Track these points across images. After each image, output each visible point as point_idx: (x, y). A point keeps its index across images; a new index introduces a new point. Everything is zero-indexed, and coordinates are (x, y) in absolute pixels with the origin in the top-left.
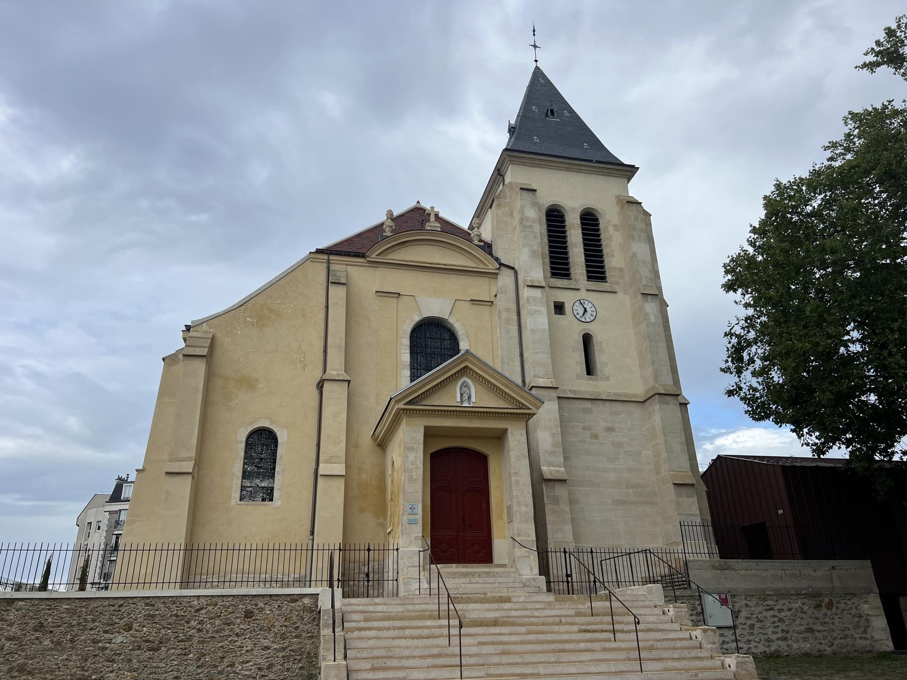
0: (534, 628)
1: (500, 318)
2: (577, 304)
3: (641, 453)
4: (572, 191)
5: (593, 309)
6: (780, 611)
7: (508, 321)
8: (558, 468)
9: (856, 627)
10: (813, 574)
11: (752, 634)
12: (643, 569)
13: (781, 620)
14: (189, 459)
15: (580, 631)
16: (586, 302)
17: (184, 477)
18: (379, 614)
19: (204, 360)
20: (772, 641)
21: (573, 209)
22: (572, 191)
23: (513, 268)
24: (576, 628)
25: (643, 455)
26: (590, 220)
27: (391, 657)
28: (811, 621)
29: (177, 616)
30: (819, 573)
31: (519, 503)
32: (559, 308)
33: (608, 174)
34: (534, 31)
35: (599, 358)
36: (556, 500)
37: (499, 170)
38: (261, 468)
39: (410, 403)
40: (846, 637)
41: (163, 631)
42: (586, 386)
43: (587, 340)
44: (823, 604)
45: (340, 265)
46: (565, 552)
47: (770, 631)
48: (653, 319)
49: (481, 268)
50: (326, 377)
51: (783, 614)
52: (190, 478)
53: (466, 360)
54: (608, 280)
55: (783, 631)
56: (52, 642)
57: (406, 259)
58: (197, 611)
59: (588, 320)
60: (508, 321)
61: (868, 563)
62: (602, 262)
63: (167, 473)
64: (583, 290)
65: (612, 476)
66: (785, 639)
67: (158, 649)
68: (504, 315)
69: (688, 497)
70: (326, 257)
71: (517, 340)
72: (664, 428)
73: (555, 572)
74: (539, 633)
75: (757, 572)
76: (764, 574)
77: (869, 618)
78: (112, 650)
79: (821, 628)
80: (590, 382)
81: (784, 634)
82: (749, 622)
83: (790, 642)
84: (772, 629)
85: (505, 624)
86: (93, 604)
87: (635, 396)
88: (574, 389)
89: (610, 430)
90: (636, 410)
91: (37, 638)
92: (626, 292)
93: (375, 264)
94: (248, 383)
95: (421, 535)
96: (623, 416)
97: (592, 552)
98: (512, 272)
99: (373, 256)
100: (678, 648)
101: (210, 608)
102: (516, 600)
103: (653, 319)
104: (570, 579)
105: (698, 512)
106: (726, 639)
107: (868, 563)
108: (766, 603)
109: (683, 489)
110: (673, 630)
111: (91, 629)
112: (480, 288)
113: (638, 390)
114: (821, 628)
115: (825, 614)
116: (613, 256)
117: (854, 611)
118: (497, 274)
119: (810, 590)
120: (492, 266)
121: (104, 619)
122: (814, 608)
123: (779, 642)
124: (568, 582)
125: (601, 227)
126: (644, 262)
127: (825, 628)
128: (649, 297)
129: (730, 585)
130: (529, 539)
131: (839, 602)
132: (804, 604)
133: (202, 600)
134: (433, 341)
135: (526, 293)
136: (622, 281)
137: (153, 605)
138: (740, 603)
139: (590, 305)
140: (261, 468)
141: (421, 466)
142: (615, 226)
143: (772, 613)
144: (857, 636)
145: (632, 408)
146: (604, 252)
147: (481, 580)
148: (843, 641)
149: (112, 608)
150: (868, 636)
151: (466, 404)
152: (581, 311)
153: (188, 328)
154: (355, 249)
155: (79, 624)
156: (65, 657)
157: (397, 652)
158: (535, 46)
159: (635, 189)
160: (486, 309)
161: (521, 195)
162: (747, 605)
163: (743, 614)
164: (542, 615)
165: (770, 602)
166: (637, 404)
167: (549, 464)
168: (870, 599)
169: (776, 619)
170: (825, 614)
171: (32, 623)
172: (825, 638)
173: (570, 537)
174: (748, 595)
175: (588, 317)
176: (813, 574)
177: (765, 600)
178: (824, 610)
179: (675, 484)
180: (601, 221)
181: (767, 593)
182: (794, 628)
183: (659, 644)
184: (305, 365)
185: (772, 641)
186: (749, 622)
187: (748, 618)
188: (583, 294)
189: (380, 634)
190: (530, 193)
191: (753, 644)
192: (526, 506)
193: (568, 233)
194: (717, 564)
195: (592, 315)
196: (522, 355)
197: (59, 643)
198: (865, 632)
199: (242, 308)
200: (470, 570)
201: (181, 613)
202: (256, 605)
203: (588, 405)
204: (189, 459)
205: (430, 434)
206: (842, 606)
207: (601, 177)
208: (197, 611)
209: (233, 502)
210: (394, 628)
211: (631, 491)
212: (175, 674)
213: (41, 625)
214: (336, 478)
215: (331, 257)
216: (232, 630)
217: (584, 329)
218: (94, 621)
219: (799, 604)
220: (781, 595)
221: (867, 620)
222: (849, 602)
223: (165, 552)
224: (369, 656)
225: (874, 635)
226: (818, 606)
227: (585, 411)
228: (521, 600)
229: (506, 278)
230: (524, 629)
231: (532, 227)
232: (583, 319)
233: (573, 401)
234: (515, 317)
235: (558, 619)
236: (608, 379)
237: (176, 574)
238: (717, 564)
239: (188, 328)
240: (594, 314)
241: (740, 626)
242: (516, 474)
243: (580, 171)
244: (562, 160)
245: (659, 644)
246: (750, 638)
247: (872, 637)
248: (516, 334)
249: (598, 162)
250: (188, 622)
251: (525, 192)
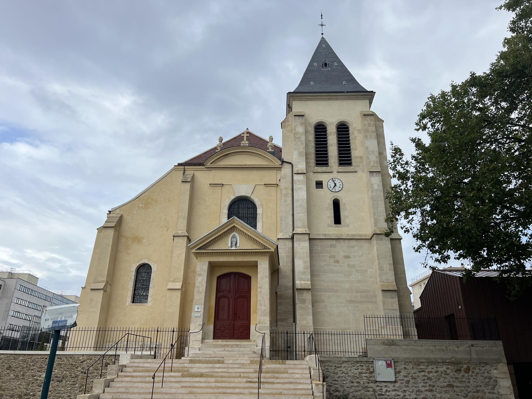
0: (219, 379)
1: (281, 193)
2: (331, 181)
3: (366, 271)
4: (330, 112)
6: (429, 372)
7: (286, 195)
8: (306, 282)
9: (487, 385)
10: (457, 349)
11: (407, 386)
12: (363, 343)
13: (429, 378)
14: (103, 282)
15: (247, 382)
17: (99, 291)
18: (142, 369)
19: (113, 229)
20: (422, 392)
21: (332, 123)
22: (330, 112)
23: (290, 163)
24: (244, 380)
25: (368, 272)
26: (343, 130)
27: (127, 393)
28: (451, 380)
29: (72, 365)
30: (461, 348)
31: (261, 305)
32: (319, 184)
33: (356, 98)
34: (322, 16)
35: (343, 214)
36: (303, 301)
37: (289, 105)
38: (143, 285)
39: (200, 249)
40: (478, 391)
41: (65, 372)
42: (334, 231)
43: (336, 204)
44: (462, 369)
45: (190, 171)
46: (287, 333)
47: (420, 385)
48: (376, 187)
49: (271, 164)
51: (431, 375)
52: (102, 292)
53: (233, 222)
54: (353, 164)
55: (430, 385)
56: (14, 375)
57: (226, 164)
58: (82, 362)
59: (337, 190)
61: (500, 343)
63: (92, 289)
64: (335, 173)
65: (347, 286)
66: (431, 391)
67: (62, 381)
68: (284, 192)
69: (391, 298)
70: (183, 167)
71: (291, 206)
72: (378, 255)
73: (300, 344)
74: (222, 382)
75: (414, 347)
76: (420, 348)
77: (498, 379)
78: (40, 381)
79: (459, 384)
80: (336, 228)
81: (431, 388)
82: (406, 379)
83: (434, 393)
84: (422, 384)
85: (212, 376)
86: (34, 358)
87: (365, 235)
89: (347, 257)
91: (8, 373)
92: (363, 171)
93: (210, 168)
94: (138, 240)
95: (201, 323)
97: (304, 333)
98: (290, 165)
99: (208, 164)
100: (298, 395)
101: (88, 361)
102: (227, 362)
103: (376, 187)
104: (289, 349)
105: (398, 308)
106: (388, 389)
107: (500, 343)
108: (419, 367)
109: (389, 294)
110: (306, 383)
111: (32, 370)
112: (270, 177)
113: (368, 232)
114: (459, 384)
115: (463, 376)
116: (356, 149)
117: (486, 374)
118: (281, 167)
119: (453, 359)
120: (278, 163)
121: (38, 365)
122: (455, 371)
123: (427, 393)
124: (287, 351)
125: (350, 132)
126: (373, 152)
127: (462, 385)
128: (375, 174)
129: (395, 355)
130: (265, 325)
131: (474, 368)
132: (448, 368)
133: (85, 357)
134: (243, 209)
135: (296, 177)
136: (361, 164)
137: (61, 359)
138: (401, 366)
139: (339, 181)
140: (143, 285)
141: (205, 284)
142: (358, 130)
143: (423, 373)
144: (487, 391)
146: (352, 147)
147: (230, 349)
148: (475, 394)
149: (42, 360)
150: (496, 391)
151: (234, 248)
152: (333, 185)
153: (110, 212)
154: (197, 162)
155: (27, 367)
156: (19, 383)
157: (131, 390)
158: (322, 25)
159: (376, 107)
160: (274, 189)
162: (405, 368)
163: (403, 373)
164: (234, 371)
165: (422, 367)
166: (366, 241)
167: (301, 279)
168: (499, 367)
169: (426, 378)
170: (463, 376)
171: (6, 366)
172: (462, 391)
173: (311, 323)
174: (407, 362)
175: (337, 189)
176: (457, 349)
177: (418, 365)
178: (463, 373)
179: (383, 290)
181: (421, 361)
182: (438, 384)
183: (286, 392)
184: (168, 228)
185: (422, 392)
186: (406, 379)
187: (405, 376)
188: (334, 175)
189: (133, 379)
190: (300, 118)
191: (407, 393)
192: (265, 306)
193: (328, 138)
194: (386, 342)
195: (340, 187)
197: (17, 376)
198: (493, 388)
199: (137, 199)
200: (232, 343)
201: (74, 363)
202: (111, 360)
203: (334, 242)
204: (103, 282)
205: (212, 267)
206: (477, 370)
207: (351, 101)
208: (82, 362)
209: (127, 304)
210: (140, 377)
211: (359, 294)
212: (69, 394)
213: (10, 367)
214: (176, 291)
215: (186, 167)
216: (98, 372)
218: (33, 366)
219: (444, 368)
220: (430, 362)
221: (496, 381)
222: (483, 369)
223: (86, 332)
224: (116, 391)
225: (500, 391)
226: (458, 371)
227: (331, 246)
228: (230, 362)
229: (286, 169)
230: (213, 380)
232: (334, 190)
233: (324, 241)
234: (290, 192)
235: (239, 374)
236: (348, 226)
237: (92, 343)
238: (386, 342)
239: (110, 212)
240: (341, 186)
241: (399, 382)
242: (260, 287)
243: (337, 99)
244: (324, 94)
245: (286, 392)
246: (406, 389)
247: (499, 392)
248: (291, 203)
249: (347, 92)
250: (77, 368)
251: (297, 117)
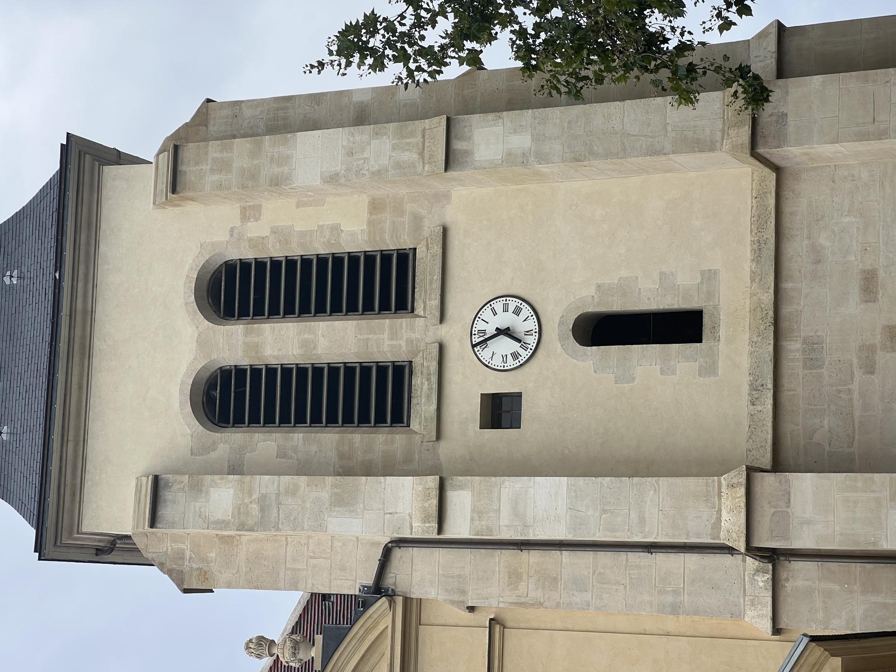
2: (485, 354)
4: (150, 348)
5: (498, 305)
16: (480, 325)
21: (202, 343)
26: (235, 290)
32: (500, 411)
33: (91, 227)
35: (649, 298)
37: (99, 551)
50: (742, 548)
54: (407, 245)
59: (532, 324)
60: (551, 581)
62: (353, 259)
64: (444, 332)
68: (530, 589)
71: (605, 558)
72: (862, 137)
80: (722, 333)
87: (759, 197)
88: (746, 388)
90: (805, 198)
92: (443, 198)
96: (823, 240)
98: (399, 554)
116: (336, 229)
120: (382, 618)
125: (249, 255)
128: (457, 145)
135: (459, 526)
136: (409, 207)
139: (487, 313)
142: (244, 218)
145: (798, 208)
146: (323, 250)
152: (505, 345)
159: (137, 127)
161: (173, 525)
166: (786, 193)
175: (524, 324)
180: (234, 254)
188: (455, 334)
195: (517, 311)
196: (651, 547)
203: (793, 348)
207: (103, 248)
217: (562, 338)
227: (813, 361)
229: (417, 573)
231: (263, 498)
232: (532, 340)
233: (785, 395)
234: (533, 557)
236: (710, 276)
240: (513, 303)
243: (89, 314)
244: (60, 376)
249: (59, 265)
